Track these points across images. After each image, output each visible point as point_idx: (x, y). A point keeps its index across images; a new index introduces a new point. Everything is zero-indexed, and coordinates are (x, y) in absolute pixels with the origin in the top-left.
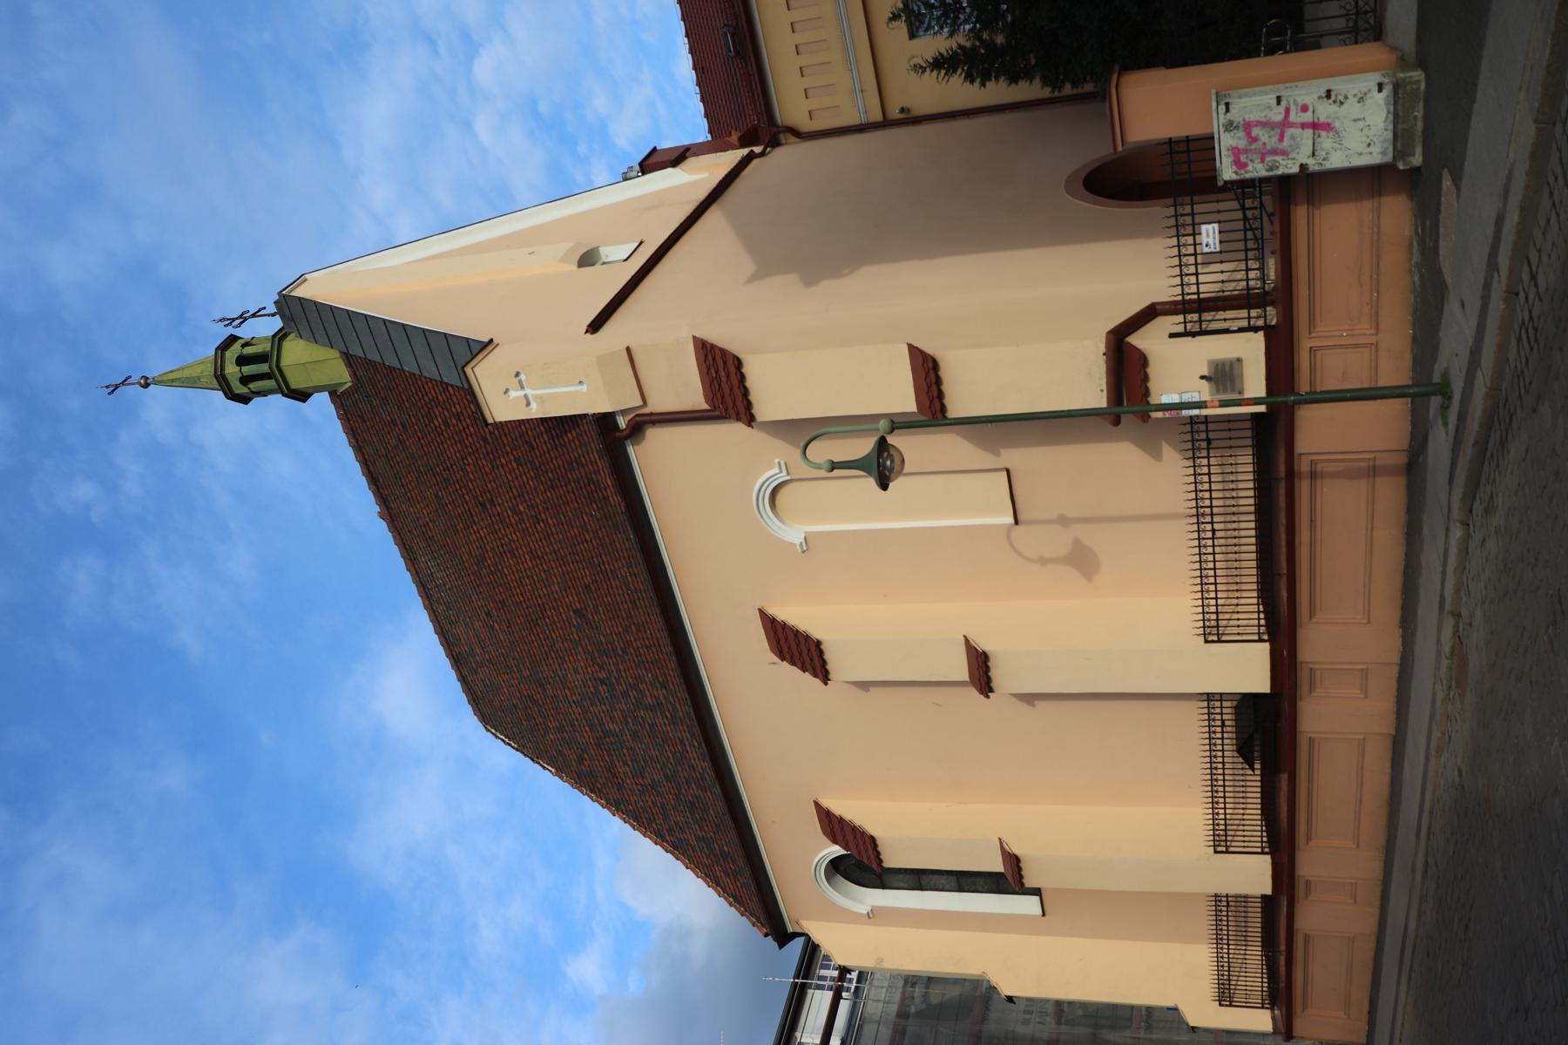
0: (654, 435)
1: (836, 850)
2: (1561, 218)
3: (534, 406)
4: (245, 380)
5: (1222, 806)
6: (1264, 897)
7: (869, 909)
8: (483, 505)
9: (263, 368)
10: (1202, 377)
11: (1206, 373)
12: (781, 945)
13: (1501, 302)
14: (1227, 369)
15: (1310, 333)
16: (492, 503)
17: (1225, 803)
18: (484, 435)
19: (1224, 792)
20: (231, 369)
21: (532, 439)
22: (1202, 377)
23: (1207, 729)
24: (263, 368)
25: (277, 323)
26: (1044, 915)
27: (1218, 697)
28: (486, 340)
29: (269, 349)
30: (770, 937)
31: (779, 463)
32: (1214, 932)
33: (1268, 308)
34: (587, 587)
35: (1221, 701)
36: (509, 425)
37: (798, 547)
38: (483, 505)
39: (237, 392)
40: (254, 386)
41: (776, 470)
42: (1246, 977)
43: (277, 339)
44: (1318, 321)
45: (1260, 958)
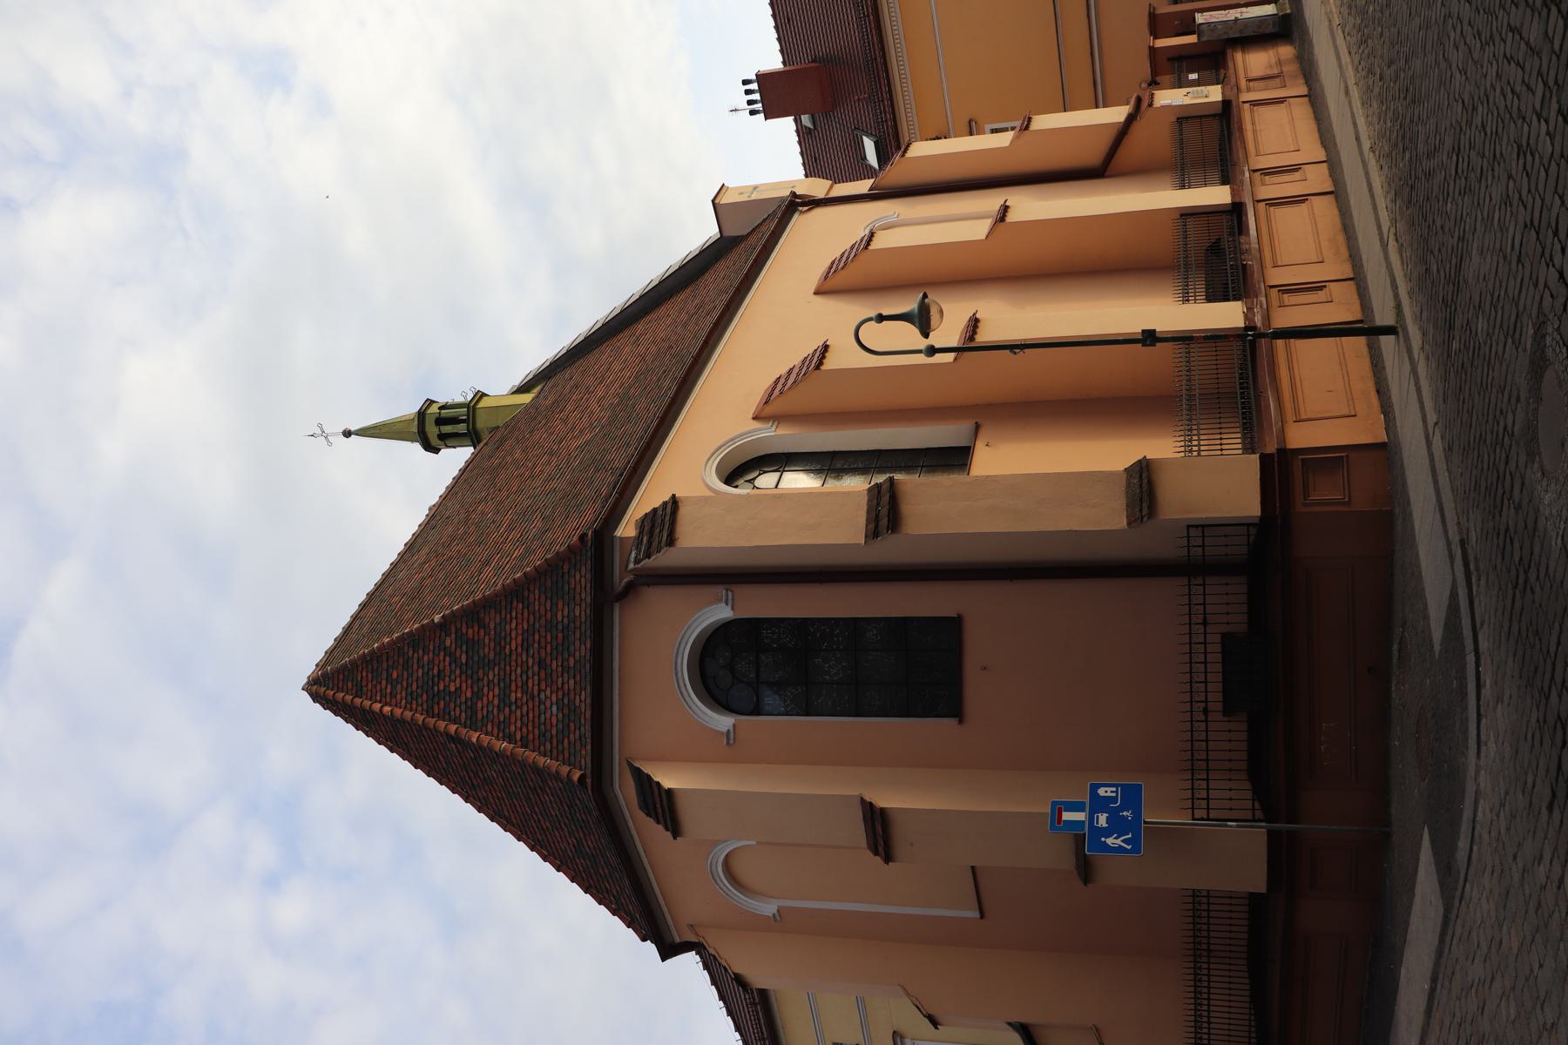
2: (1535, 790)
5: (1205, 920)
6: (1253, 897)
12: (665, 956)
17: (1209, 981)
19: (1209, 944)
23: (1191, 926)
27: (1205, 893)
32: (1191, 920)
35: (1208, 896)
42: (1230, 1024)
45: (1247, 1017)
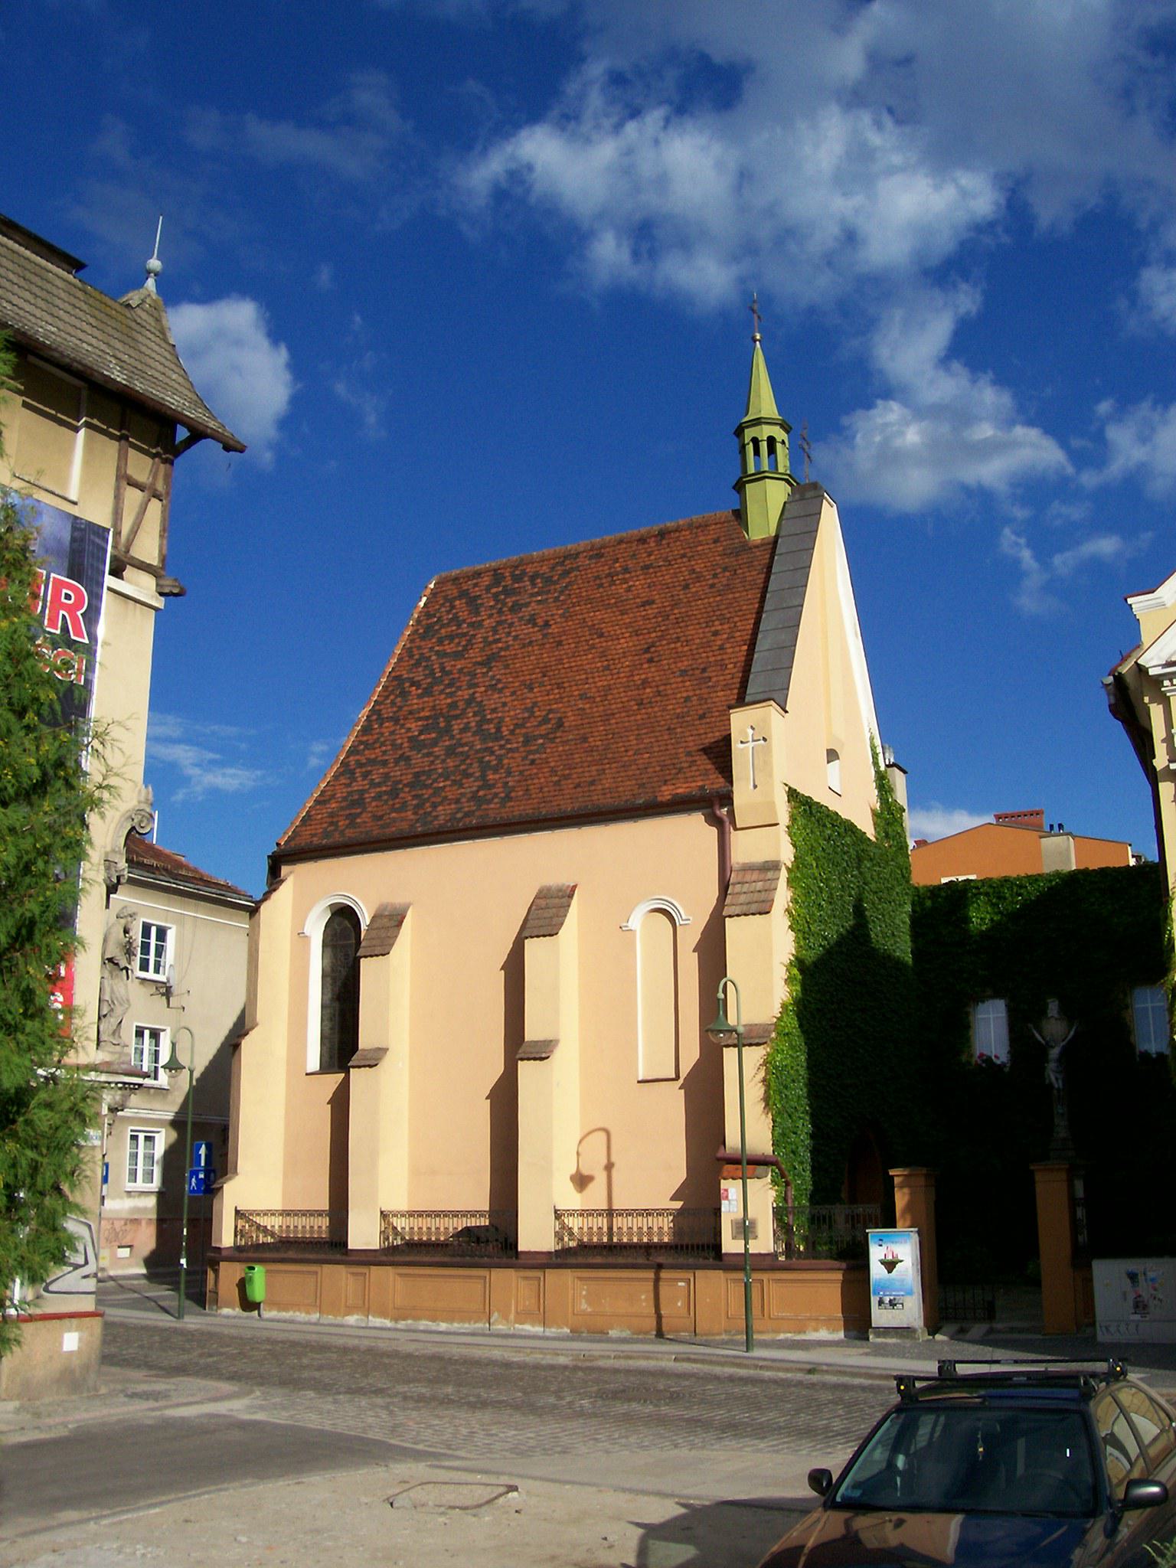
1: (365, 920)
3: (742, 746)
4: (756, 441)
8: (647, 650)
13: (76, 1425)
16: (650, 661)
21: (708, 720)
24: (765, 466)
26: (307, 1074)
28: (787, 709)
29: (780, 471)
30: (275, 849)
33: (1122, 1496)
36: (725, 718)
37: (625, 924)
38: (647, 650)
41: (684, 917)
43: (787, 477)
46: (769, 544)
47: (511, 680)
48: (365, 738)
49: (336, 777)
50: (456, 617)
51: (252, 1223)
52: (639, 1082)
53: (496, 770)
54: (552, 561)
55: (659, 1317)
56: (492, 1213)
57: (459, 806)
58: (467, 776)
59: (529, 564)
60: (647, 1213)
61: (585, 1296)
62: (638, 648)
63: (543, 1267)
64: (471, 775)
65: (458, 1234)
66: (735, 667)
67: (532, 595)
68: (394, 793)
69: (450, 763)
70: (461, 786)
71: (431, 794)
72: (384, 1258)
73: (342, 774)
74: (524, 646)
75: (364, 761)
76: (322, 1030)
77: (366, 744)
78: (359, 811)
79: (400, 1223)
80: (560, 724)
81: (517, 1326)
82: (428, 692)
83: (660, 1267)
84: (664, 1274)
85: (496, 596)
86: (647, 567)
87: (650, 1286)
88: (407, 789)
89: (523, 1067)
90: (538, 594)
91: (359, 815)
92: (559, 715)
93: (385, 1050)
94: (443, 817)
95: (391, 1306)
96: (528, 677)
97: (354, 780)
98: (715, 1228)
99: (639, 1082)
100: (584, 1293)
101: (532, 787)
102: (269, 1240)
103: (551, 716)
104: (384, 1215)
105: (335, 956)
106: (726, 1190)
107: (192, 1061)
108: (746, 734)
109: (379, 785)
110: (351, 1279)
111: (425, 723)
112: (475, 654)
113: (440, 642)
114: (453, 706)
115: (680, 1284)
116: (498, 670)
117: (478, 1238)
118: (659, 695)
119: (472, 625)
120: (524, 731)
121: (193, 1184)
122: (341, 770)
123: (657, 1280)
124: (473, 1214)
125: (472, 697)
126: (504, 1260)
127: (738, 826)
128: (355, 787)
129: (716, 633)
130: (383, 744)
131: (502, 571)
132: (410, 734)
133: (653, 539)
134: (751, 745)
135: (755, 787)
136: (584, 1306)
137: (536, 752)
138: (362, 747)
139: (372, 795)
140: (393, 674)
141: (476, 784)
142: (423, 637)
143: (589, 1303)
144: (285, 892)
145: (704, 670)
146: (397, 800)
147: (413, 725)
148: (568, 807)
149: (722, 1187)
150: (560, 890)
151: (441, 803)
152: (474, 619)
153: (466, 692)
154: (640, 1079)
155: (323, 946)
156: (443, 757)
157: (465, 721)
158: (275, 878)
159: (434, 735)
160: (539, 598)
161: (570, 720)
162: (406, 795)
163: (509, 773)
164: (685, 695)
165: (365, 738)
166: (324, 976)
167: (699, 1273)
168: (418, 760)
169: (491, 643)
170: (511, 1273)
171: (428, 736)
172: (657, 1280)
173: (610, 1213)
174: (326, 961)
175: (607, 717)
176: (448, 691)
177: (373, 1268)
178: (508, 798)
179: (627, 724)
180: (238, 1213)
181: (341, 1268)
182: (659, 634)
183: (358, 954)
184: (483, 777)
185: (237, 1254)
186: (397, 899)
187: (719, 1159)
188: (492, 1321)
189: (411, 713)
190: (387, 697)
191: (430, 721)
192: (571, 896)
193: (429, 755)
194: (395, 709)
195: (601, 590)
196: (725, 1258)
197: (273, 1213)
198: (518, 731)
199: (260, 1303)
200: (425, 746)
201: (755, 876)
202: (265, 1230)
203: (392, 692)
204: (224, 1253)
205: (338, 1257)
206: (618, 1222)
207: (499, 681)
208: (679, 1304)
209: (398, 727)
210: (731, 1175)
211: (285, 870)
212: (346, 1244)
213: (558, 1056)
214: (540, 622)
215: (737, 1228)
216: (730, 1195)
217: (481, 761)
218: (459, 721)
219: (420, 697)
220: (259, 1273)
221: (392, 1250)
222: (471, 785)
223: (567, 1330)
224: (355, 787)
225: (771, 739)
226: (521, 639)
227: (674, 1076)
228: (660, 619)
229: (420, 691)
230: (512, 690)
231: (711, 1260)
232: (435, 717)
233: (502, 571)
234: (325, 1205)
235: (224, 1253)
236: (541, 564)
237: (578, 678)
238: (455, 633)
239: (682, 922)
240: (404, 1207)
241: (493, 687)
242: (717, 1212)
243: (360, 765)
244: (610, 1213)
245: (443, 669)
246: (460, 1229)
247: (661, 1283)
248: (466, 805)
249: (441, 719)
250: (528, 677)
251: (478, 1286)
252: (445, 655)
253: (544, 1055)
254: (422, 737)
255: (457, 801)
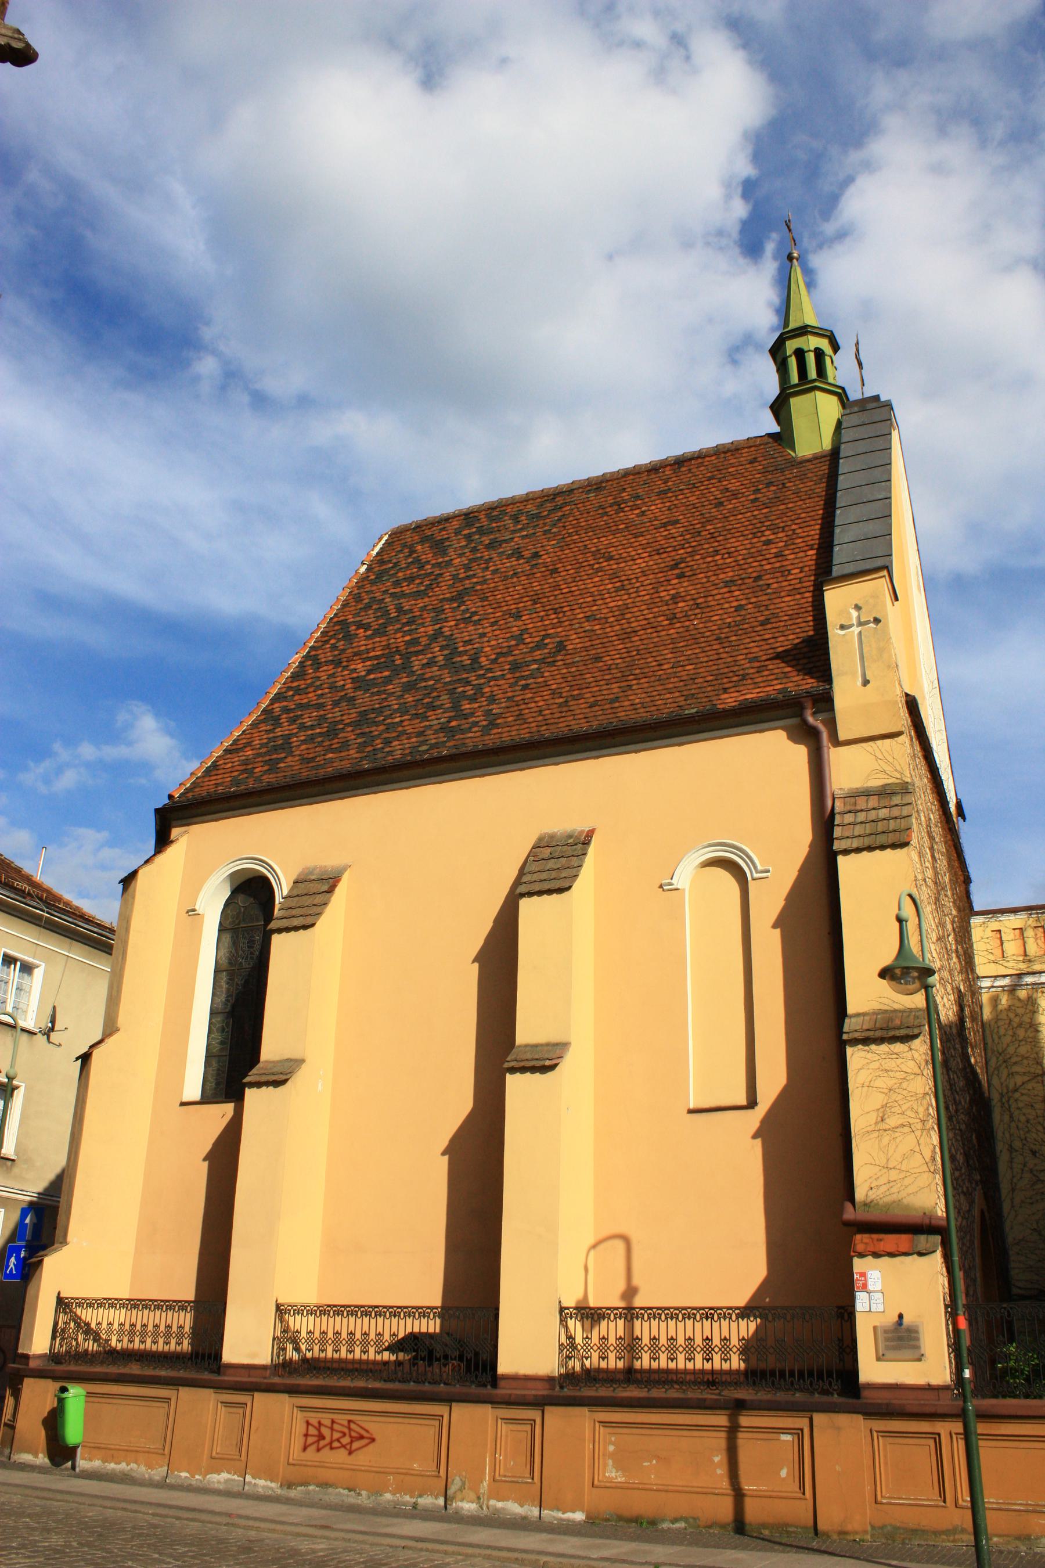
0: (800, 753)
1: (282, 888)
4: (800, 354)
7: (200, 912)
8: (676, 566)
9: (812, 374)
10: (901, 1316)
11: (906, 1320)
14: (912, 1343)
15: (599, 1422)
16: (679, 577)
18: (763, 578)
20: (813, 342)
22: (901, 1316)
24: (812, 374)
25: (854, 395)
26: (183, 1104)
30: (167, 801)
31: (768, 871)
34: (597, 659)
38: (676, 566)
39: (788, 343)
40: (793, 362)
41: (760, 868)
44: (511, 1427)
46: (824, 457)
47: (491, 611)
48: (295, 684)
49: (254, 725)
50: (417, 560)
51: (77, 1319)
52: (691, 1111)
53: (473, 699)
54: (539, 500)
55: (739, 1495)
56: (446, 1312)
57: (422, 739)
58: (432, 707)
59: (509, 505)
60: (709, 1313)
61: (612, 1455)
62: (663, 565)
63: (540, 1403)
64: (440, 707)
65: (398, 1346)
66: (801, 572)
67: (514, 532)
68: (332, 732)
69: (409, 698)
70: (426, 718)
71: (383, 730)
72: (276, 1380)
73: (263, 721)
74: (506, 578)
75: (293, 707)
76: (208, 1046)
77: (298, 691)
78: (283, 755)
79: (301, 1324)
80: (561, 647)
81: (492, 1502)
82: (380, 632)
83: (739, 1406)
84: (745, 1420)
85: (468, 537)
86: (665, 492)
87: (720, 1440)
88: (350, 729)
89: (514, 1083)
90: (522, 529)
91: (282, 760)
92: (558, 639)
93: (303, 1061)
94: (399, 752)
95: (283, 1458)
96: (513, 606)
97: (280, 725)
98: (841, 1340)
99: (691, 1111)
100: (611, 1448)
101: (527, 711)
102: (91, 1346)
103: (546, 641)
104: (281, 1311)
105: (235, 943)
106: (863, 1275)
107: (13, 1064)
108: (850, 618)
109: (312, 727)
110: (222, 1410)
111: (376, 662)
112: (444, 590)
113: (397, 584)
114: (415, 642)
115: (784, 1437)
116: (472, 604)
117: (431, 1353)
118: (698, 608)
119: (438, 565)
120: (511, 658)
121: (12, 1265)
122: (263, 717)
123: (733, 1431)
124: (422, 1312)
125: (439, 633)
126: (474, 1389)
127: (842, 736)
128: (279, 732)
129: (768, 542)
130: (320, 687)
131: (476, 514)
132: (355, 675)
133: (668, 468)
134: (856, 630)
135: (866, 682)
136: (612, 1473)
137: (531, 676)
138: (291, 693)
139: (303, 738)
140: (335, 620)
141: (446, 715)
142: (373, 583)
143: (618, 1467)
144: (175, 853)
145: (758, 578)
146: (336, 741)
147: (360, 666)
148: (580, 725)
149: (856, 1270)
150: (570, 836)
151: (397, 738)
152: (441, 560)
153: (431, 628)
154: (692, 1106)
155: (219, 931)
156: (399, 693)
157: (430, 655)
158: (163, 841)
159: (387, 673)
160: (525, 533)
161: (574, 642)
162: (349, 734)
163: (492, 699)
164: (735, 604)
165: (295, 684)
166: (217, 971)
167: (819, 1418)
168: (365, 700)
169: (462, 580)
170: (486, 1413)
171: (379, 675)
172: (733, 1431)
173: (630, 1313)
174: (222, 953)
175: (626, 636)
176: (406, 629)
177: (257, 1395)
178: (492, 724)
179: (656, 640)
180: (62, 1304)
181: (208, 1394)
182: (689, 550)
183: (269, 927)
184: (456, 706)
185: (53, 1366)
186: (327, 860)
187: (848, 1224)
188: (450, 1492)
189: (356, 654)
190: (326, 642)
191: (382, 660)
192: (586, 843)
193: (378, 693)
194: (336, 653)
195: (605, 518)
196: (865, 1393)
197: (111, 1303)
198: (501, 660)
199: (74, 1449)
200: (375, 685)
201: (873, 802)
202: (87, 1330)
203: (332, 637)
204: (33, 1364)
205: (206, 1376)
206: (644, 1329)
207: (475, 613)
208: (784, 1473)
209: (340, 669)
210: (871, 1248)
211: (175, 832)
212: (218, 1355)
213: (567, 1065)
214: (527, 554)
215: (887, 1340)
216: (870, 1282)
217: (452, 692)
218: (421, 657)
219: (368, 638)
220: (76, 1396)
221: (285, 1367)
222: (437, 718)
223: (579, 1516)
224: (279, 732)
225: (887, 619)
226: (502, 573)
227: (743, 1101)
228: (688, 536)
229: (369, 633)
230: (493, 620)
231: (836, 1396)
232: (391, 655)
233: (476, 514)
234: (188, 1292)
235: (33, 1364)
236: (525, 503)
237: (581, 601)
238: (415, 575)
239: (756, 875)
240: (311, 1298)
241: (467, 621)
242: (847, 1314)
243: (286, 710)
244: (630, 1313)
245: (400, 609)
246: (401, 1335)
247: (740, 1435)
248: (432, 737)
249: (398, 657)
250: (513, 606)
251: (427, 1432)
252: (403, 595)
253: (547, 1063)
254: (372, 676)
255: (421, 734)
